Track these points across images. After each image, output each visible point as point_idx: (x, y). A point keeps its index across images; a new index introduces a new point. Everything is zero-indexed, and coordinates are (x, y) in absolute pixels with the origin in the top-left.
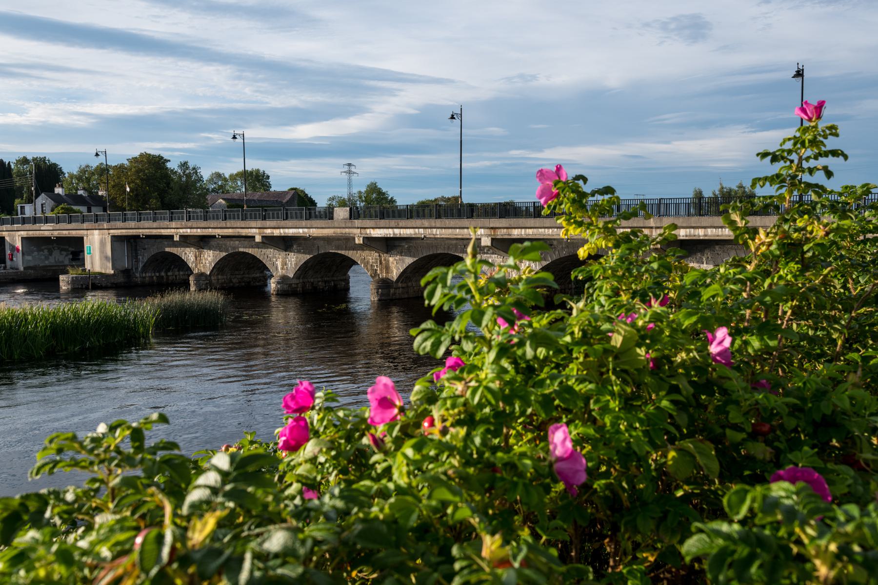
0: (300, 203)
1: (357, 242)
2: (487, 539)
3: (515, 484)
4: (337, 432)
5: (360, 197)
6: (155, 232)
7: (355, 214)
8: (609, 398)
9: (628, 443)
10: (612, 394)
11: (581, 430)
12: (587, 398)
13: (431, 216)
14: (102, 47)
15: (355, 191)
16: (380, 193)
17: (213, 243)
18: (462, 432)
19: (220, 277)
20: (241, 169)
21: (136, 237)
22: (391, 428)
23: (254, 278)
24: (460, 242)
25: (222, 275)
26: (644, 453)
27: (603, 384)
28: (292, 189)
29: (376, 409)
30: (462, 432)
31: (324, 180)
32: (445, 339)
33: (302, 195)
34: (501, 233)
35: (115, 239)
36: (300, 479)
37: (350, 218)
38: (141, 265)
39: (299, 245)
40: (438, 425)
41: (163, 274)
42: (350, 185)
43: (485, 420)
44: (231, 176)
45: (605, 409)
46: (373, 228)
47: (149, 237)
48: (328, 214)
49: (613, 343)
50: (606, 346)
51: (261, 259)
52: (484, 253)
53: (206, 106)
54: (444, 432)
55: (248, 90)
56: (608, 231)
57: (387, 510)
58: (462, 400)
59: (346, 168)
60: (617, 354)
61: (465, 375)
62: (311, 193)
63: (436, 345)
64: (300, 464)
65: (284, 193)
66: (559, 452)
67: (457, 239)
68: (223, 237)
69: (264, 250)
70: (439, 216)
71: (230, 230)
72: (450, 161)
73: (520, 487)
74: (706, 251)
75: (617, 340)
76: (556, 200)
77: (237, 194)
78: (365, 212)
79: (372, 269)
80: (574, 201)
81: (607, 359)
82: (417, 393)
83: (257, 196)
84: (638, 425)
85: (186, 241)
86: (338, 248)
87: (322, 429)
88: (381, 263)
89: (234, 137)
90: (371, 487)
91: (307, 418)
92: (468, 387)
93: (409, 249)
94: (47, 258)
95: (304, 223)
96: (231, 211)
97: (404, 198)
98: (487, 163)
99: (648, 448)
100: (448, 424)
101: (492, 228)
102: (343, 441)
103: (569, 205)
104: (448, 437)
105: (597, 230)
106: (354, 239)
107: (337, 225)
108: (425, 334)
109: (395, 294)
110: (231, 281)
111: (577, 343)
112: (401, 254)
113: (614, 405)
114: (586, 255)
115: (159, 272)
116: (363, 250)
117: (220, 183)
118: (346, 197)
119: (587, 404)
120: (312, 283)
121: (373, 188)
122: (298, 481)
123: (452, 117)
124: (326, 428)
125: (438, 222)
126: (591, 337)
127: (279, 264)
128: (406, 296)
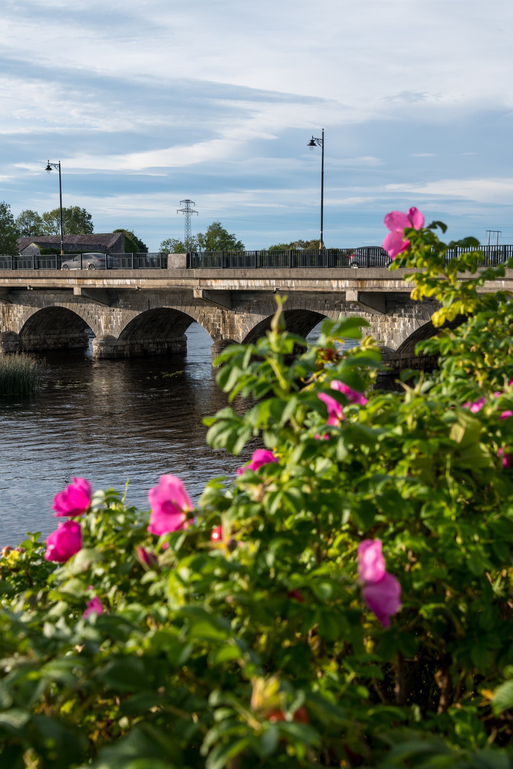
0: (127, 249)
1: (195, 295)
2: (259, 684)
3: (312, 613)
4: (118, 539)
5: (201, 241)
7: (193, 261)
8: (443, 504)
9: (464, 559)
10: (449, 500)
11: (408, 543)
12: (417, 503)
13: (285, 265)
15: (194, 233)
16: (224, 235)
17: (23, 296)
18: (253, 547)
19: (32, 337)
20: (57, 207)
22: (174, 539)
23: (72, 339)
24: (321, 297)
25: (35, 334)
26: (482, 572)
27: (437, 487)
28: (118, 231)
29: (158, 514)
30: (253, 547)
31: (158, 222)
32: (243, 433)
33: (130, 238)
34: (370, 286)
36: (67, 597)
37: (188, 267)
39: (126, 299)
40: (227, 538)
42: (188, 226)
43: (285, 534)
44: (45, 215)
45: (439, 518)
46: (215, 279)
48: (161, 261)
49: (452, 437)
50: (445, 441)
51: (81, 315)
52: (350, 310)
53: (23, 130)
54: (232, 546)
55: (74, 112)
56: (466, 294)
57: (146, 643)
58: (257, 508)
59: (184, 206)
60: (458, 451)
61: (265, 476)
62: (141, 235)
63: (233, 439)
64: (68, 579)
65: (108, 236)
66: (369, 574)
67: (316, 293)
68: (35, 289)
69: (84, 305)
70: (295, 265)
71: (44, 281)
72: (308, 197)
73: (318, 616)
75: (458, 433)
76: (406, 252)
77: (52, 237)
78: (206, 259)
79: (214, 329)
80: (427, 256)
81: (444, 455)
82: (207, 497)
83: (76, 239)
84: (476, 538)
86: (172, 303)
87: (99, 537)
88: (224, 321)
89: (49, 168)
90: (139, 613)
91: (83, 524)
92: (266, 492)
93: (258, 304)
95: (132, 272)
96: (44, 258)
97: (253, 242)
98: (358, 200)
99: (487, 566)
100: (238, 536)
101: (359, 279)
102: (122, 551)
103: (421, 260)
104: (235, 553)
105: (453, 293)
106: (192, 291)
107: (171, 275)
108: (222, 425)
110: (45, 342)
111: (408, 436)
113: (450, 513)
114: (442, 321)
116: (203, 305)
117: (32, 224)
118: (183, 242)
119: (418, 511)
120: (142, 345)
121: (216, 230)
122: (64, 600)
123: (312, 143)
124: (105, 534)
125: (294, 272)
126: (428, 429)
127: (102, 321)
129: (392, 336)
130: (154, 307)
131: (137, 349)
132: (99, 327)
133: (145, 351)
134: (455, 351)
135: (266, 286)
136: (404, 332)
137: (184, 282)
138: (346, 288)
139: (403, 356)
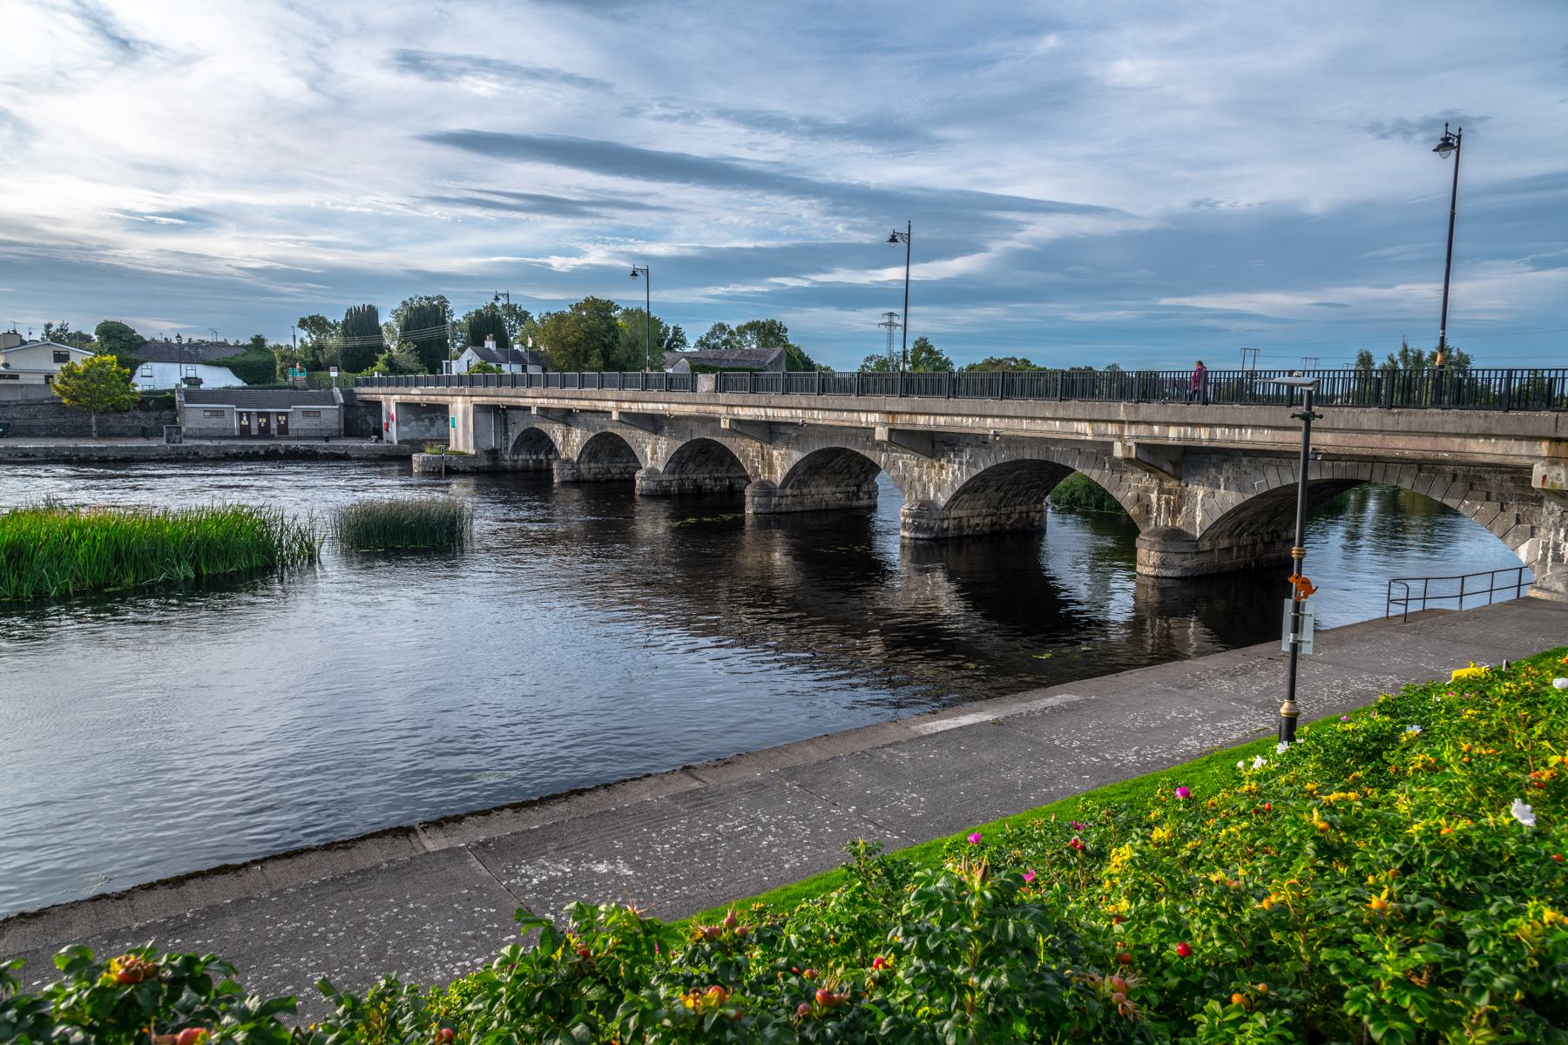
6: (514, 401)
14: (685, 181)
16: (930, 351)
34: (902, 422)
35: (479, 408)
38: (511, 445)
41: (542, 457)
71: (587, 403)
72: (1427, 291)
74: (1226, 466)
93: (797, 438)
94: (428, 430)
109: (779, 505)
110: (609, 471)
115: (537, 453)
117: (724, 337)
121: (923, 345)
123: (893, 239)
125: (819, 401)
127: (648, 450)
128: (799, 508)
129: (938, 488)
130: (696, 437)
133: (699, 488)
136: (953, 483)
137: (712, 408)
139: (954, 513)
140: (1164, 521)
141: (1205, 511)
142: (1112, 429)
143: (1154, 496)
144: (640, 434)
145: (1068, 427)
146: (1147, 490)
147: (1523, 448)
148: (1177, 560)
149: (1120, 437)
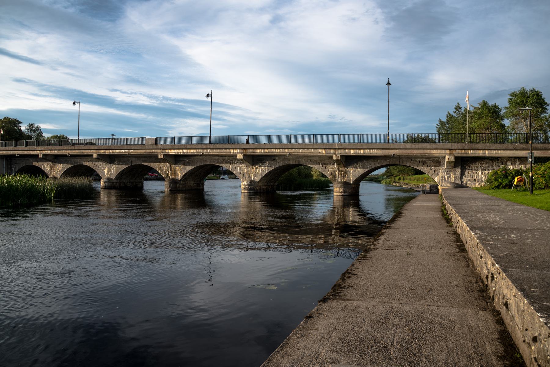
1: (159, 157)
21: (13, 156)
24: (221, 158)
46: (170, 149)
47: (21, 156)
51: (94, 168)
85: (46, 158)
86: (144, 162)
88: (171, 170)
89: (74, 104)
109: (179, 187)
112: (184, 165)
127: (106, 171)
129: (255, 175)
131: (122, 185)
132: (104, 174)
134: (405, 167)
135: (197, 152)
136: (262, 174)
138: (238, 153)
139: (260, 184)
140: (341, 180)
141: (353, 176)
142: (332, 151)
143: (337, 173)
144: (100, 164)
145: (317, 151)
146: (334, 171)
147: (443, 152)
148: (347, 190)
149: (335, 153)
